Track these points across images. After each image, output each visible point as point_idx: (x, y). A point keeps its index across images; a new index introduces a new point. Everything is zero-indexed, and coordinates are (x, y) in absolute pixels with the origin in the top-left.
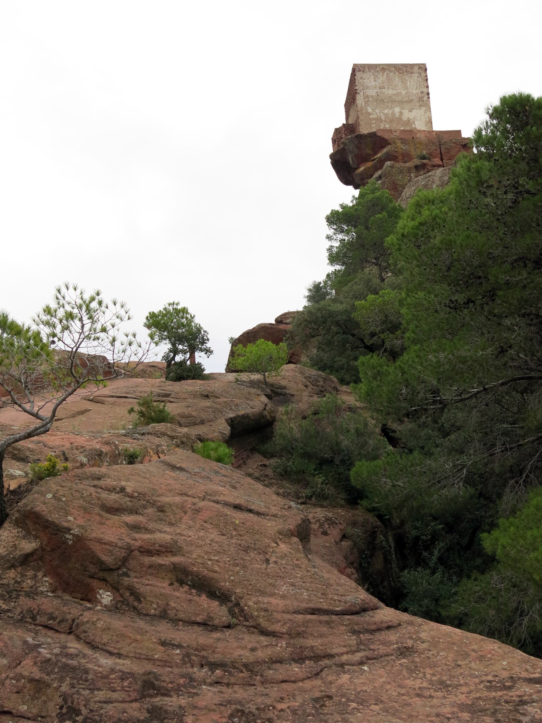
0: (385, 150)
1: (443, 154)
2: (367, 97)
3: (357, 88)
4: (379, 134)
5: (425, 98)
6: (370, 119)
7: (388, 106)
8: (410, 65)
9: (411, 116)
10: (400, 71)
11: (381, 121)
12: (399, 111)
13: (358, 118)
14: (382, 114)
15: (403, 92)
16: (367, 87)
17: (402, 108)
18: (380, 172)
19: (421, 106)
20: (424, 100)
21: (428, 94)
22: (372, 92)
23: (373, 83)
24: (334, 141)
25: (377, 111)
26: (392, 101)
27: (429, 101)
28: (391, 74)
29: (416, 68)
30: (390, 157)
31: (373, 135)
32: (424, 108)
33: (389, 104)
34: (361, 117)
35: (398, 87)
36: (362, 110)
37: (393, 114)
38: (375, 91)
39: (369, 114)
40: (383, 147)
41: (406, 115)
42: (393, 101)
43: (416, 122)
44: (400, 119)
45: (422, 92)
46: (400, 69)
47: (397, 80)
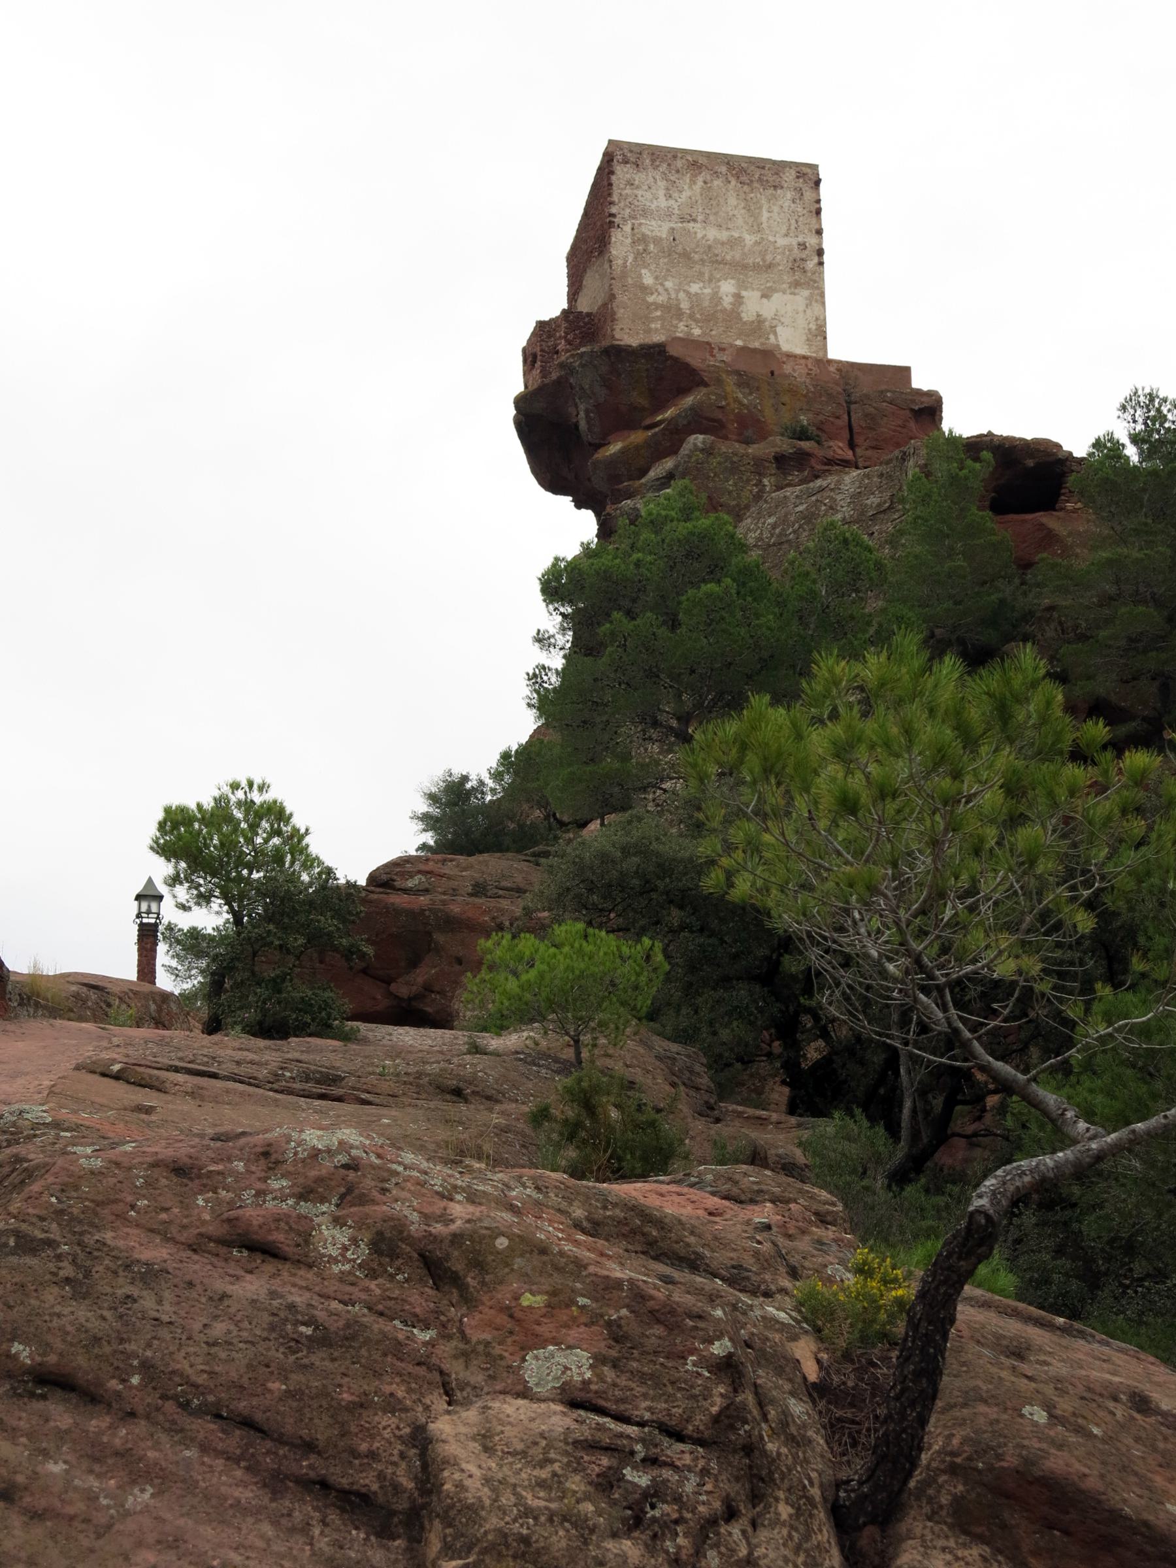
0: (689, 400)
1: (856, 429)
2: (644, 239)
3: (614, 210)
4: (673, 351)
5: (811, 264)
6: (649, 305)
7: (701, 274)
8: (774, 162)
9: (767, 309)
10: (744, 178)
11: (679, 314)
13: (612, 297)
14: (682, 295)
15: (749, 239)
16: (645, 213)
17: (742, 285)
18: (669, 463)
19: (797, 284)
20: (806, 268)
21: (820, 252)
22: (658, 229)
23: (663, 203)
24: (530, 358)
25: (669, 284)
26: (715, 261)
28: (717, 183)
29: (789, 176)
30: (699, 421)
31: (655, 353)
34: (622, 298)
35: (734, 224)
36: (624, 275)
37: (716, 298)
39: (645, 289)
40: (684, 391)
41: (754, 306)
42: (717, 262)
43: (779, 329)
44: (733, 316)
45: (803, 246)
46: (743, 170)
47: (733, 201)
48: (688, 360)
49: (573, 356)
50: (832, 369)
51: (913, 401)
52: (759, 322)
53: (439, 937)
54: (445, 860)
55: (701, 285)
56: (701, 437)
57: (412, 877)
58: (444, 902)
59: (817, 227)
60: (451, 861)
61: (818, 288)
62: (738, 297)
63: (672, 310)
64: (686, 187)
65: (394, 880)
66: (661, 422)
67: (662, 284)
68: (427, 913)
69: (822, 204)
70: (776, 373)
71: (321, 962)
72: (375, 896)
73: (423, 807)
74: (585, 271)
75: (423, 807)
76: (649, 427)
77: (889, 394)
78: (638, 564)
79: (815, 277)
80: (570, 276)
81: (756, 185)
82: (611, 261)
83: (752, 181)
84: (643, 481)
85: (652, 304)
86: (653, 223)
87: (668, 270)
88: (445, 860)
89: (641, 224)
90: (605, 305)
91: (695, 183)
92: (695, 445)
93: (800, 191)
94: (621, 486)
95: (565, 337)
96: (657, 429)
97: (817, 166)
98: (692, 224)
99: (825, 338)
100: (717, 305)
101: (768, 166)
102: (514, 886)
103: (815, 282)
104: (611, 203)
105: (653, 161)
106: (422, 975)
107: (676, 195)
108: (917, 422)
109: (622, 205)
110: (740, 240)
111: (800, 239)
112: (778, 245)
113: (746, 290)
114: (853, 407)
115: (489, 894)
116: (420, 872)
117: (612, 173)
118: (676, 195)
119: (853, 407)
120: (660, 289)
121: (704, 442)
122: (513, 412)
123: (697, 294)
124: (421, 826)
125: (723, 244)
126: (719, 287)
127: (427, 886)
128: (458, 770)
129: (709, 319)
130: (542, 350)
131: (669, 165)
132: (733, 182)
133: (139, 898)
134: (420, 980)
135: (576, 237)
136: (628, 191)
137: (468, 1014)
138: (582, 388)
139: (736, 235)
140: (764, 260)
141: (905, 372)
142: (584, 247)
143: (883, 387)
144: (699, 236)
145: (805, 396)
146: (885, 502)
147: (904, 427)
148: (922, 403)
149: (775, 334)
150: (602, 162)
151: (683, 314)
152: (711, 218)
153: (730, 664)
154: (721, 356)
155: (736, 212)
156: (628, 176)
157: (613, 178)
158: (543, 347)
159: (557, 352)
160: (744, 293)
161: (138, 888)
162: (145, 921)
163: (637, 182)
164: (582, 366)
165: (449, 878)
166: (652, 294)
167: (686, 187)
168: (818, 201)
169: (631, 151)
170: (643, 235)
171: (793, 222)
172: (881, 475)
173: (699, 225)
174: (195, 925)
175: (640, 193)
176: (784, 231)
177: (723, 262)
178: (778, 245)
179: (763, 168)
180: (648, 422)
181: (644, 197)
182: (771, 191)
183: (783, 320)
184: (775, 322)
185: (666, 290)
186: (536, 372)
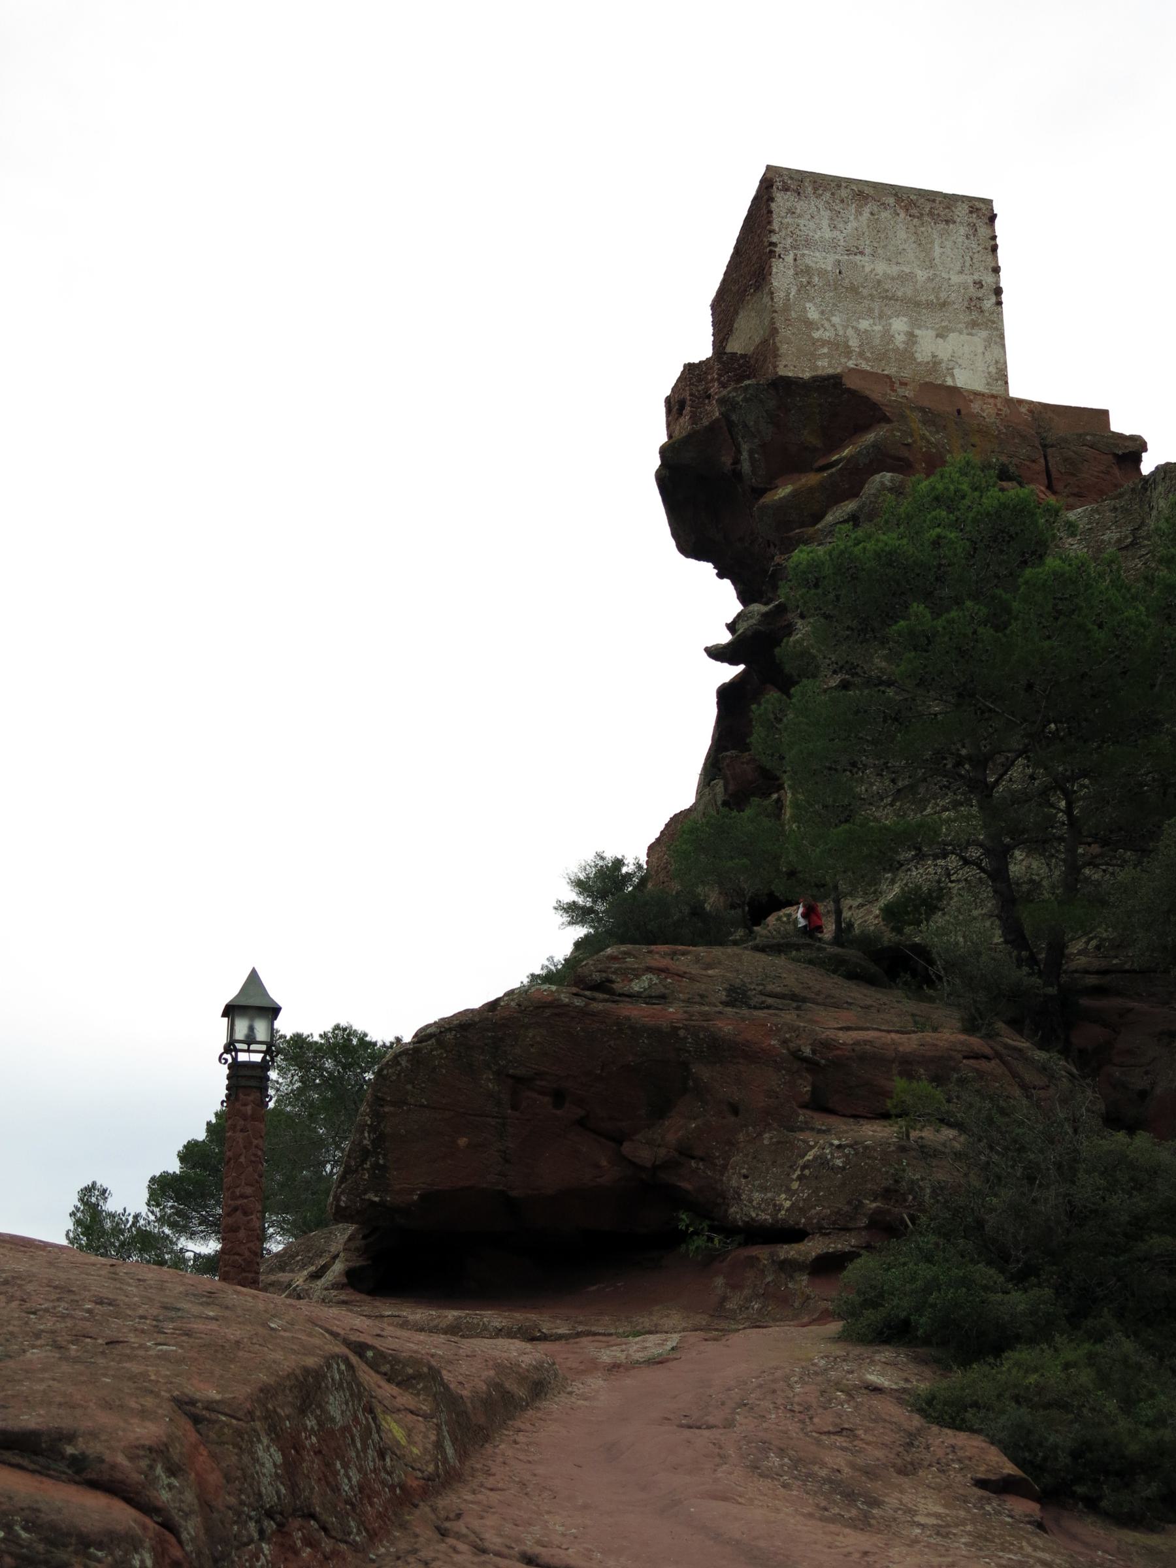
0: (870, 437)
1: (1054, 474)
2: (808, 271)
3: (774, 239)
4: (851, 383)
5: (989, 303)
6: (814, 342)
7: (871, 310)
8: (945, 196)
9: (944, 349)
10: (914, 211)
11: (848, 352)
12: (905, 328)
13: (774, 331)
14: (850, 332)
15: (921, 275)
16: (808, 243)
17: (915, 323)
18: (850, 506)
19: (974, 324)
20: (983, 306)
21: (998, 291)
22: (821, 260)
23: (828, 234)
24: (675, 406)
25: (836, 320)
26: (886, 297)
27: (1000, 314)
28: (885, 215)
29: (962, 211)
30: (881, 459)
31: (831, 385)
32: (984, 334)
33: (876, 306)
34: (785, 332)
35: (899, 259)
36: (787, 308)
37: (887, 336)
38: (831, 258)
39: (810, 324)
40: (865, 428)
41: (928, 346)
42: (889, 298)
43: (956, 371)
44: (906, 355)
45: (979, 284)
46: (912, 203)
47: (902, 234)
48: (867, 393)
49: (735, 389)
50: (1023, 410)
51: (1116, 445)
52: (935, 363)
53: (703, 1072)
54: (675, 953)
55: (871, 321)
56: (889, 475)
57: (638, 977)
58: (706, 1017)
59: (993, 264)
60: (683, 954)
61: (997, 329)
62: (911, 335)
63: (840, 347)
64: (852, 218)
65: (612, 982)
66: (837, 462)
67: (828, 320)
68: (682, 1033)
69: (998, 241)
70: (963, 412)
71: (514, 1107)
72: (600, 1006)
73: (571, 896)
74: (736, 313)
75: (571, 896)
76: (822, 469)
77: (1088, 438)
78: (936, 543)
79: (994, 317)
80: (715, 324)
81: (926, 218)
82: (772, 293)
83: (922, 215)
84: (819, 526)
85: (818, 340)
86: (817, 254)
87: (834, 305)
88: (675, 953)
89: (803, 255)
90: (765, 342)
91: (861, 214)
92: (882, 483)
93: (974, 227)
94: (791, 534)
95: (718, 379)
96: (834, 470)
97: (991, 201)
98: (859, 257)
99: (1006, 383)
100: (888, 344)
101: (938, 199)
102: (785, 991)
103: (994, 322)
104: (771, 232)
105: (815, 189)
106: (675, 1129)
107: (841, 226)
108: (1120, 469)
109: (783, 233)
110: (911, 276)
111: (976, 277)
112: (952, 282)
113: (919, 328)
114: (1049, 450)
115: (752, 1003)
116: (649, 969)
117: (772, 199)
118: (841, 226)
119: (1049, 450)
120: (827, 324)
121: (892, 481)
122: (657, 462)
123: (866, 331)
124: (566, 919)
125: (893, 279)
126: (890, 324)
127: (663, 990)
128: (610, 854)
129: (882, 357)
130: (691, 395)
131: (833, 194)
132: (902, 215)
133: (230, 1011)
134: (672, 1138)
135: (724, 282)
136: (789, 220)
137: (757, 1196)
138: (745, 426)
139: (907, 270)
140: (938, 298)
141: (1104, 414)
142: (735, 288)
143: (1081, 431)
144: (867, 269)
145: (997, 437)
146: (1126, 537)
147: (1108, 473)
148: (1126, 447)
149: (953, 376)
150: (758, 191)
151: (851, 352)
152: (880, 251)
153: (1084, 675)
154: (901, 391)
155: (906, 247)
156: (789, 204)
157: (773, 205)
158: (690, 394)
159: (709, 397)
160: (917, 332)
161: (230, 991)
162: (243, 1057)
163: (798, 211)
164: (746, 400)
165: (693, 979)
166: (818, 329)
167: (852, 218)
168: (994, 238)
169: (791, 178)
170: (807, 266)
171: (968, 258)
172: (1115, 509)
173: (866, 259)
174: (300, 1031)
175: (802, 222)
176: (958, 268)
177: (894, 298)
178: (952, 282)
179: (934, 201)
180: (822, 462)
181: (807, 226)
182: (942, 226)
183: (960, 361)
184: (951, 364)
185: (833, 326)
186: (685, 419)
